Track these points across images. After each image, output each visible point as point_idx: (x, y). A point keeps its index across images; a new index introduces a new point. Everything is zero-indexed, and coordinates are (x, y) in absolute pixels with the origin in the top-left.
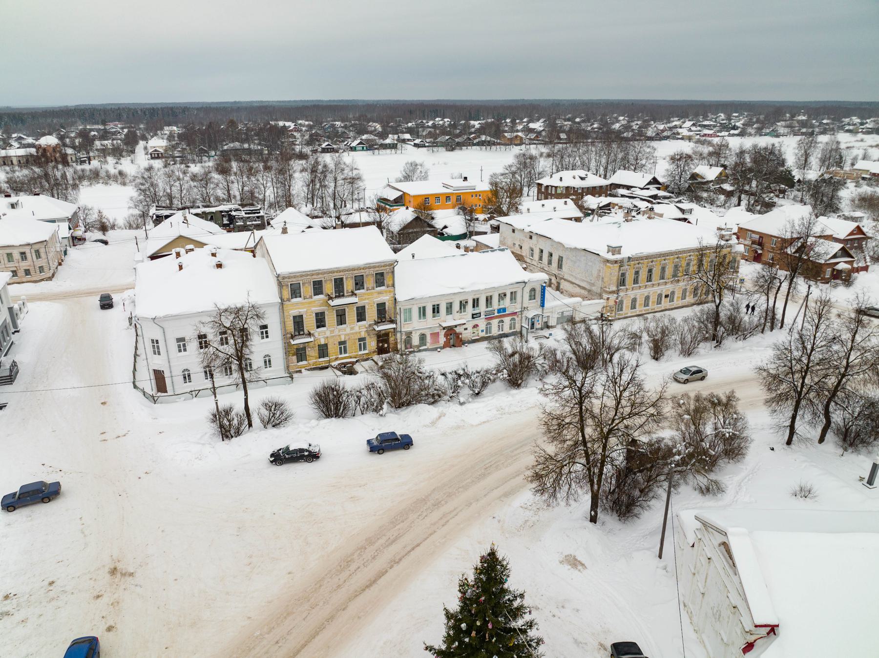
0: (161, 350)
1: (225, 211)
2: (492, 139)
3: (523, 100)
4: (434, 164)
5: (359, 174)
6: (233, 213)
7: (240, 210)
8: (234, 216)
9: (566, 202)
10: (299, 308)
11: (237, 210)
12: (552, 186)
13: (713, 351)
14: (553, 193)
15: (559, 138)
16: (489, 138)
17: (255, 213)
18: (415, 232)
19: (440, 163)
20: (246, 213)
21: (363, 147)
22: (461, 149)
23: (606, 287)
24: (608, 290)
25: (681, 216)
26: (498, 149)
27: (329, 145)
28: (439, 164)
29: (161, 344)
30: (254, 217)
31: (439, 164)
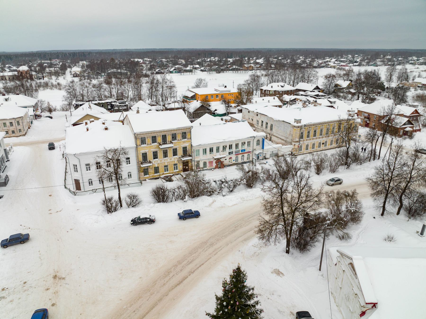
0: (78, 170)
1: (109, 103)
2: (239, 67)
3: (254, 48)
4: (210, 80)
5: (174, 84)
6: (113, 103)
7: (116, 102)
8: (114, 105)
9: (274, 98)
10: (145, 150)
11: (115, 102)
12: (268, 90)
13: (346, 170)
14: (268, 93)
15: (271, 67)
16: (237, 67)
17: (123, 103)
18: (201, 113)
19: (213, 79)
20: (119, 103)
21: (176, 71)
22: (224, 72)
23: (293, 139)
24: (294, 140)
25: (330, 105)
26: (242, 72)
27: (159, 70)
28: (213, 79)
29: (78, 167)
30: (123, 105)
31: (213, 79)
